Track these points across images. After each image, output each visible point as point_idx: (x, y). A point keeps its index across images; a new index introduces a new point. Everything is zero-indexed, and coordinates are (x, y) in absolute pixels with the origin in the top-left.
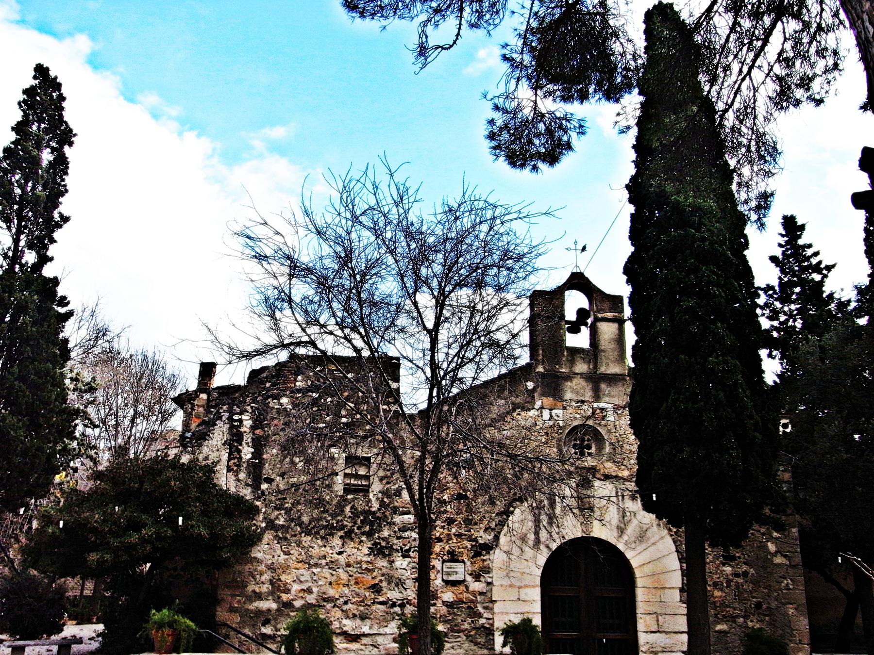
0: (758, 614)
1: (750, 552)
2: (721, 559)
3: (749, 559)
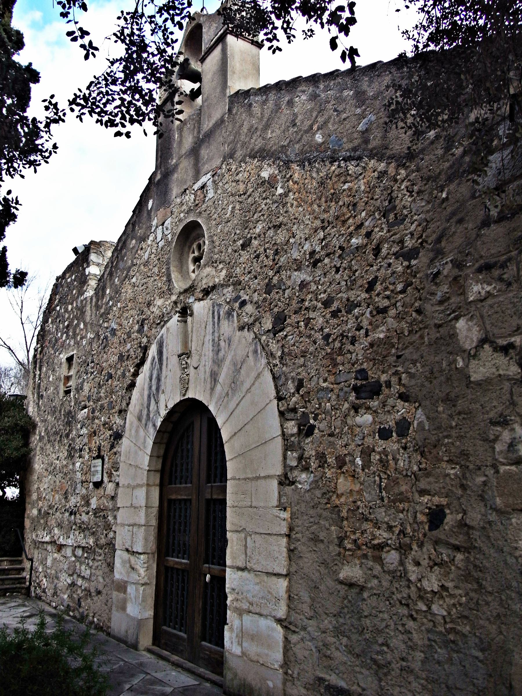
0: (437, 542)
1: (414, 362)
2: (352, 397)
3: (413, 382)
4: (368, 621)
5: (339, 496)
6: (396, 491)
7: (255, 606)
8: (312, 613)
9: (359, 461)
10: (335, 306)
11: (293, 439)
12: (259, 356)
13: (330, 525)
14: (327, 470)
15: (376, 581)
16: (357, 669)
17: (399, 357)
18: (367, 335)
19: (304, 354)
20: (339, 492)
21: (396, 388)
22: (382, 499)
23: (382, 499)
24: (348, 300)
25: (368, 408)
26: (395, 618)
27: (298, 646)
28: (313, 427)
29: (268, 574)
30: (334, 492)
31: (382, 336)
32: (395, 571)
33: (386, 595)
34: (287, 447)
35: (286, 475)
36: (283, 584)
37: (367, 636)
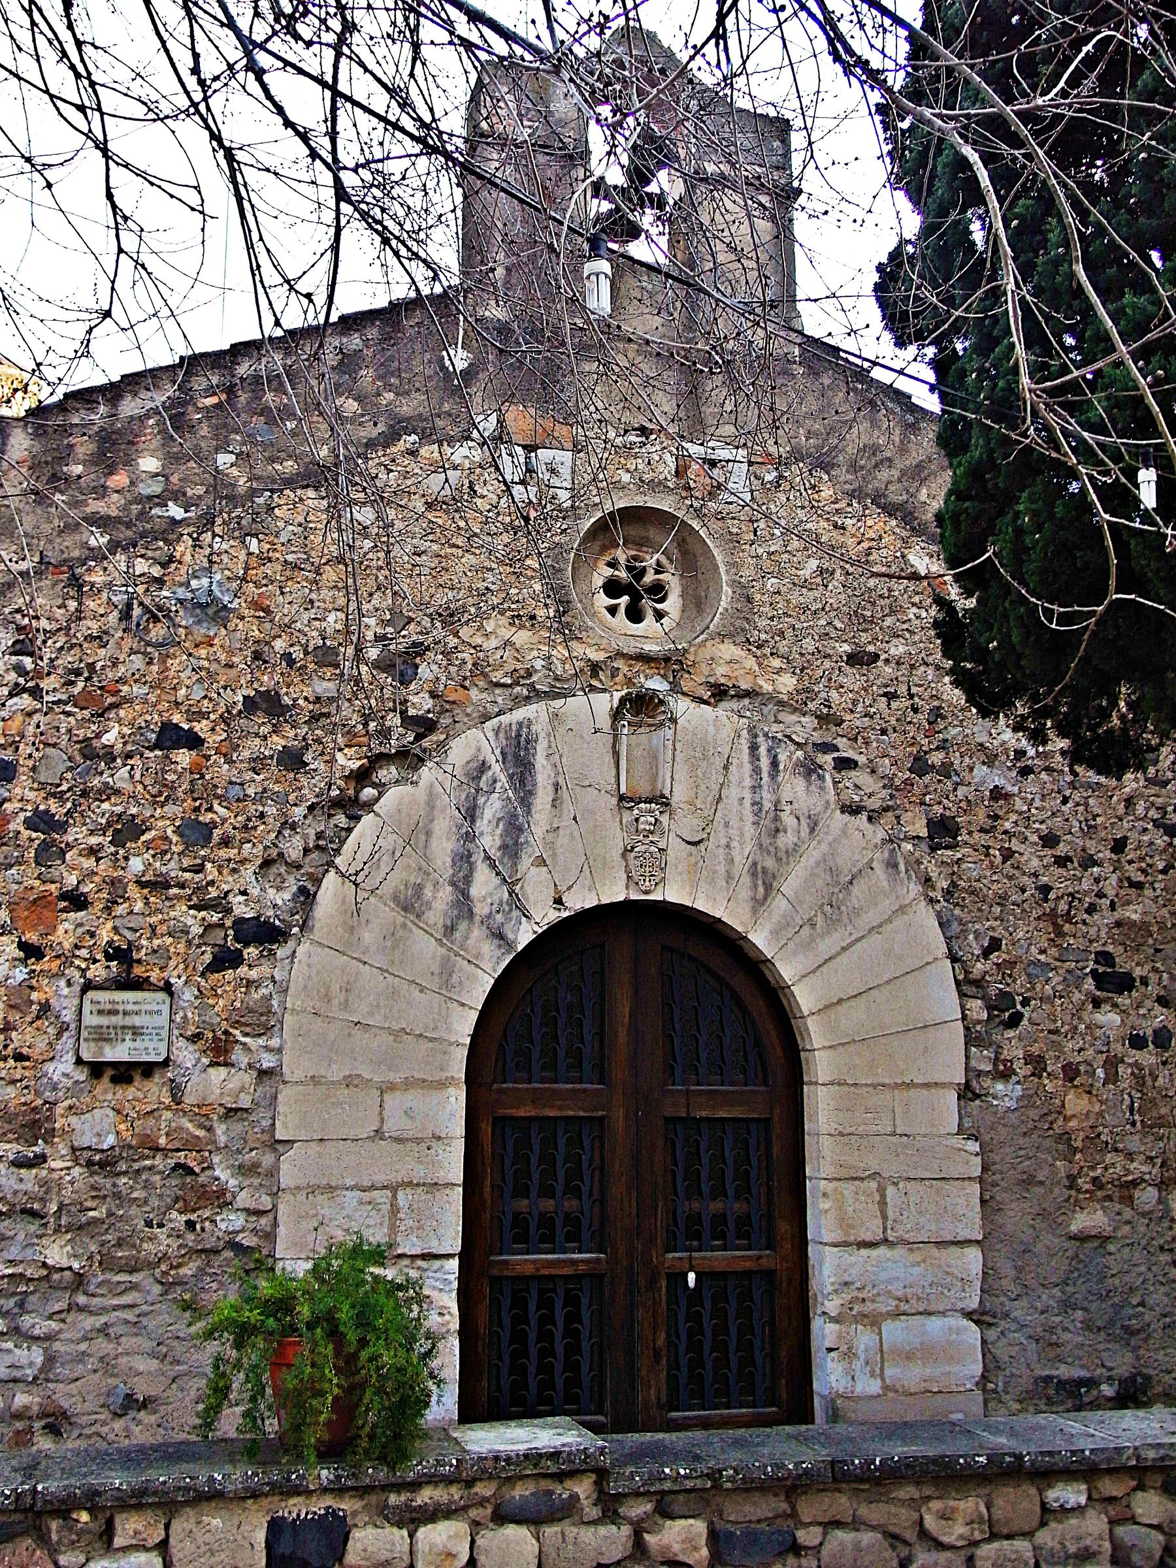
2: (1089, 984)
4: (1117, 1282)
5: (1067, 1119)
6: (1155, 1114)
7: (913, 1302)
8: (1018, 1290)
9: (1100, 1072)
10: (1062, 849)
11: (978, 1028)
12: (903, 875)
13: (1055, 1159)
14: (1046, 1082)
15: (1127, 1228)
16: (1101, 1347)
17: (1157, 951)
18: (1113, 906)
19: (1002, 900)
20: (1069, 1113)
21: (1153, 989)
22: (1133, 1124)
23: (1133, 1124)
24: (1084, 850)
25: (1115, 1005)
26: (1154, 1268)
27: (1000, 1344)
28: (1020, 1016)
29: (940, 1244)
30: (1060, 1113)
31: (1135, 917)
32: (1151, 1212)
33: (1143, 1242)
34: (972, 1038)
35: (967, 1084)
36: (973, 1258)
37: (1116, 1300)
